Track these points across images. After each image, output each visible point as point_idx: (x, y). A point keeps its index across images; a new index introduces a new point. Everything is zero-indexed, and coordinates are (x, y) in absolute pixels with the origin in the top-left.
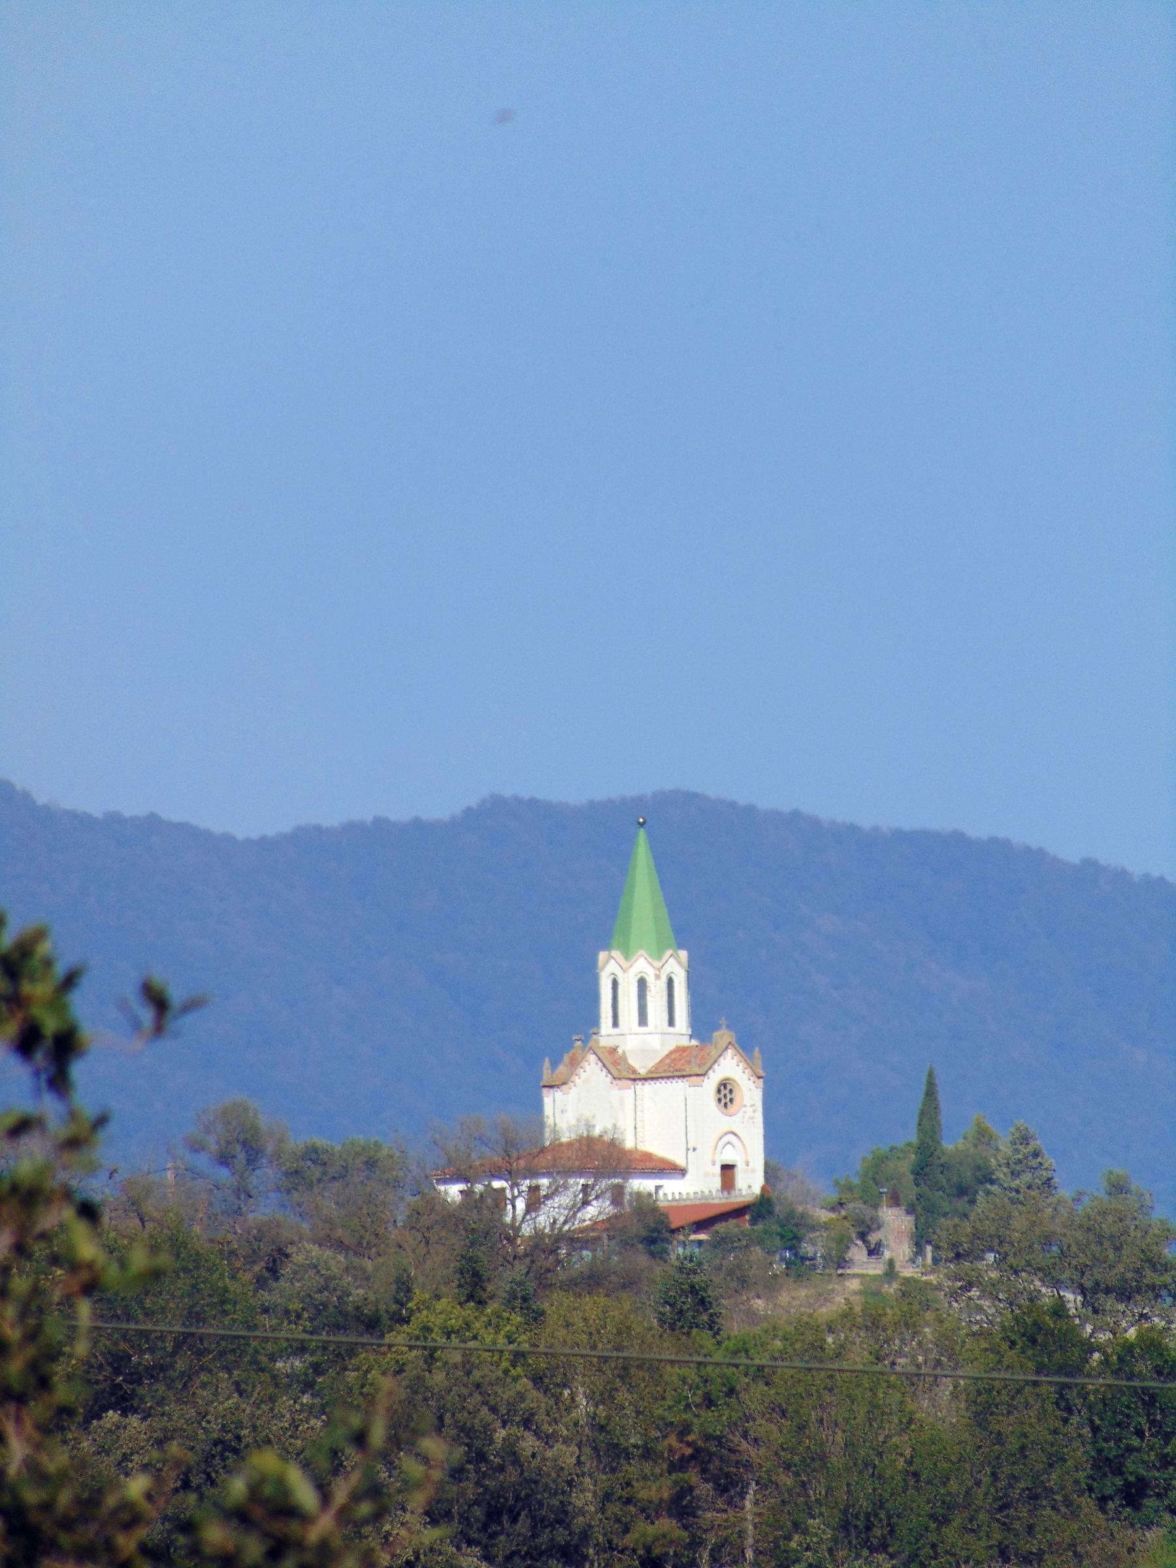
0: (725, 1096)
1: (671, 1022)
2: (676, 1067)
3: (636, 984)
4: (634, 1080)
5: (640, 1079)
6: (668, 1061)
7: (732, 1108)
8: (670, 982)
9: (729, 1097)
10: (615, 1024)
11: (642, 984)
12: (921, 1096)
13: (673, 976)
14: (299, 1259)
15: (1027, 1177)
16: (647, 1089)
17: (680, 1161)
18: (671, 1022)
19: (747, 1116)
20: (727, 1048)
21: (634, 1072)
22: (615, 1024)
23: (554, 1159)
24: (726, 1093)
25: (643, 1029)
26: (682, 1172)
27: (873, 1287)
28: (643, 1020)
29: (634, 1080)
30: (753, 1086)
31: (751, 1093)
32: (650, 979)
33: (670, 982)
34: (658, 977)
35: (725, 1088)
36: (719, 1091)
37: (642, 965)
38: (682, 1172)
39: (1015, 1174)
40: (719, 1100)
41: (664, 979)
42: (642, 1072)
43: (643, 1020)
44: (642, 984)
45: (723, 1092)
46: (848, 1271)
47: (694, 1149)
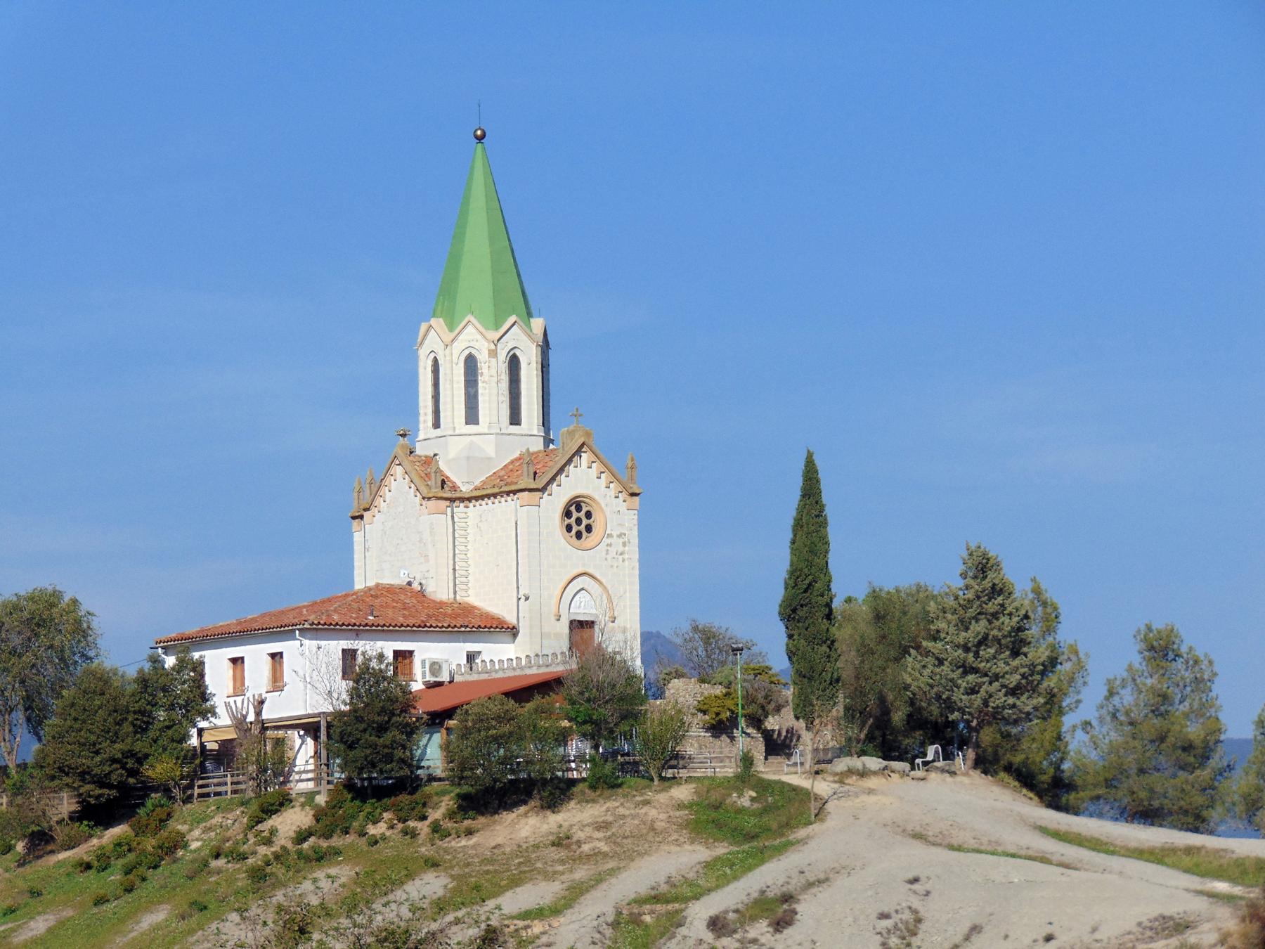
0: (579, 521)
1: (515, 419)
2: (521, 481)
3: (462, 364)
4: (452, 500)
5: (462, 500)
6: (503, 473)
7: (589, 540)
8: (514, 363)
9: (585, 521)
10: (437, 425)
11: (471, 364)
12: (797, 494)
13: (518, 353)
14: (348, 804)
15: (980, 627)
16: (474, 510)
17: (512, 620)
18: (515, 419)
19: (613, 550)
20: (578, 452)
21: (454, 488)
22: (437, 425)
23: (1202, 705)
24: (578, 518)
25: (472, 429)
26: (513, 632)
27: (715, 796)
28: (472, 416)
29: (452, 500)
30: (623, 507)
31: (617, 515)
32: (482, 357)
33: (514, 363)
34: (493, 354)
35: (579, 509)
36: (568, 514)
37: (473, 338)
38: (513, 631)
39: (964, 625)
40: (569, 528)
41: (503, 356)
42: (465, 489)
43: (472, 416)
44: (471, 364)
45: (575, 515)
46: (683, 773)
47: (527, 599)
